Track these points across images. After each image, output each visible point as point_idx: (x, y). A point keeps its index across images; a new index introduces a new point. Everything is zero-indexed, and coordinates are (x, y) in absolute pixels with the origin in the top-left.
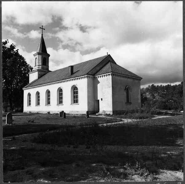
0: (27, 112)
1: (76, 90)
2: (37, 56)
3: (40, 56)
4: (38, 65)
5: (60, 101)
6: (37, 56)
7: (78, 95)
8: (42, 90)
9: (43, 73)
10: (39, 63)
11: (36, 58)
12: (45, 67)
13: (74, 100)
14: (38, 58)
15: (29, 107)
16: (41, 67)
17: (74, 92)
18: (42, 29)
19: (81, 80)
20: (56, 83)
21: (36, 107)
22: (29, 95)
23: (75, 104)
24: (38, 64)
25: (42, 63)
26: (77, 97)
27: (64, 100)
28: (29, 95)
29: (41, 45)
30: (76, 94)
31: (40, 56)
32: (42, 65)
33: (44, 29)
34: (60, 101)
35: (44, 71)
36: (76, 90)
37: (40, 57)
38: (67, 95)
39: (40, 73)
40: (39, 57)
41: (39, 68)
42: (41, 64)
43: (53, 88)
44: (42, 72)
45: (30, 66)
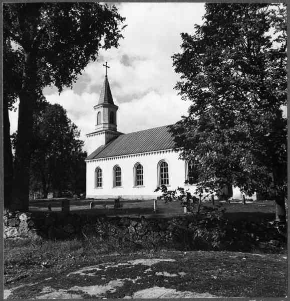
0: (94, 197)
1: (140, 168)
2: (101, 110)
3: (107, 110)
4: (104, 124)
5: (118, 183)
6: (102, 108)
7: (169, 173)
8: (108, 166)
9: (112, 136)
10: (104, 120)
11: (99, 112)
12: (113, 126)
13: (98, 184)
14: (104, 112)
15: (99, 189)
16: (107, 126)
17: (116, 173)
18: (106, 67)
19: (163, 155)
20: (127, 156)
21: (96, 190)
22: (99, 171)
23: (117, 187)
24: (102, 122)
25: (109, 121)
26: (142, 177)
27: (104, 182)
28: (99, 171)
29: (107, 93)
30: (140, 173)
31: (107, 110)
32: (109, 124)
33: (109, 67)
34: (118, 183)
35: (112, 134)
36: (140, 168)
37: (105, 111)
38: (128, 176)
39: (108, 136)
40: (104, 112)
41: (105, 129)
42: (107, 122)
43: (127, 164)
44: (110, 135)
45: (72, 123)
